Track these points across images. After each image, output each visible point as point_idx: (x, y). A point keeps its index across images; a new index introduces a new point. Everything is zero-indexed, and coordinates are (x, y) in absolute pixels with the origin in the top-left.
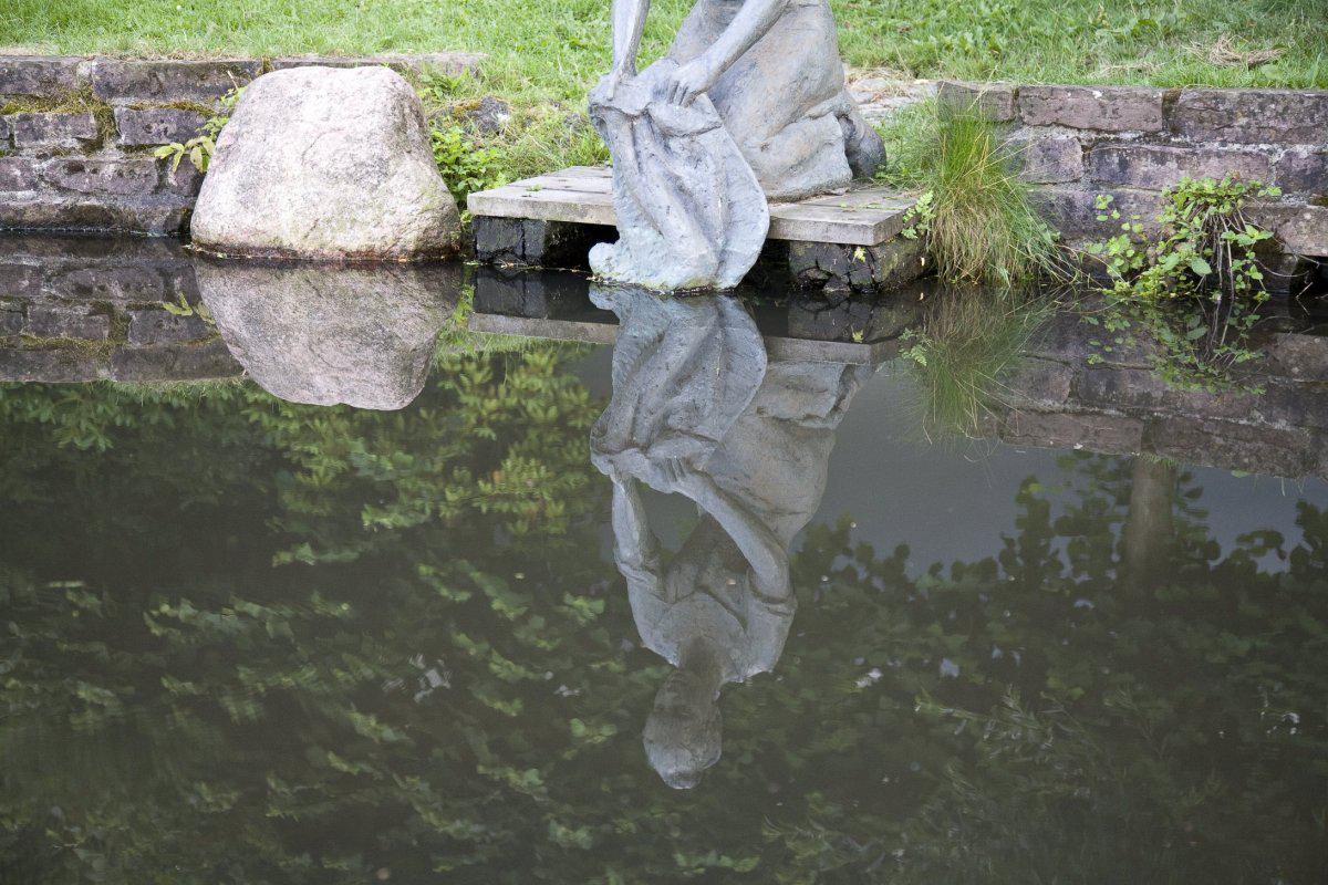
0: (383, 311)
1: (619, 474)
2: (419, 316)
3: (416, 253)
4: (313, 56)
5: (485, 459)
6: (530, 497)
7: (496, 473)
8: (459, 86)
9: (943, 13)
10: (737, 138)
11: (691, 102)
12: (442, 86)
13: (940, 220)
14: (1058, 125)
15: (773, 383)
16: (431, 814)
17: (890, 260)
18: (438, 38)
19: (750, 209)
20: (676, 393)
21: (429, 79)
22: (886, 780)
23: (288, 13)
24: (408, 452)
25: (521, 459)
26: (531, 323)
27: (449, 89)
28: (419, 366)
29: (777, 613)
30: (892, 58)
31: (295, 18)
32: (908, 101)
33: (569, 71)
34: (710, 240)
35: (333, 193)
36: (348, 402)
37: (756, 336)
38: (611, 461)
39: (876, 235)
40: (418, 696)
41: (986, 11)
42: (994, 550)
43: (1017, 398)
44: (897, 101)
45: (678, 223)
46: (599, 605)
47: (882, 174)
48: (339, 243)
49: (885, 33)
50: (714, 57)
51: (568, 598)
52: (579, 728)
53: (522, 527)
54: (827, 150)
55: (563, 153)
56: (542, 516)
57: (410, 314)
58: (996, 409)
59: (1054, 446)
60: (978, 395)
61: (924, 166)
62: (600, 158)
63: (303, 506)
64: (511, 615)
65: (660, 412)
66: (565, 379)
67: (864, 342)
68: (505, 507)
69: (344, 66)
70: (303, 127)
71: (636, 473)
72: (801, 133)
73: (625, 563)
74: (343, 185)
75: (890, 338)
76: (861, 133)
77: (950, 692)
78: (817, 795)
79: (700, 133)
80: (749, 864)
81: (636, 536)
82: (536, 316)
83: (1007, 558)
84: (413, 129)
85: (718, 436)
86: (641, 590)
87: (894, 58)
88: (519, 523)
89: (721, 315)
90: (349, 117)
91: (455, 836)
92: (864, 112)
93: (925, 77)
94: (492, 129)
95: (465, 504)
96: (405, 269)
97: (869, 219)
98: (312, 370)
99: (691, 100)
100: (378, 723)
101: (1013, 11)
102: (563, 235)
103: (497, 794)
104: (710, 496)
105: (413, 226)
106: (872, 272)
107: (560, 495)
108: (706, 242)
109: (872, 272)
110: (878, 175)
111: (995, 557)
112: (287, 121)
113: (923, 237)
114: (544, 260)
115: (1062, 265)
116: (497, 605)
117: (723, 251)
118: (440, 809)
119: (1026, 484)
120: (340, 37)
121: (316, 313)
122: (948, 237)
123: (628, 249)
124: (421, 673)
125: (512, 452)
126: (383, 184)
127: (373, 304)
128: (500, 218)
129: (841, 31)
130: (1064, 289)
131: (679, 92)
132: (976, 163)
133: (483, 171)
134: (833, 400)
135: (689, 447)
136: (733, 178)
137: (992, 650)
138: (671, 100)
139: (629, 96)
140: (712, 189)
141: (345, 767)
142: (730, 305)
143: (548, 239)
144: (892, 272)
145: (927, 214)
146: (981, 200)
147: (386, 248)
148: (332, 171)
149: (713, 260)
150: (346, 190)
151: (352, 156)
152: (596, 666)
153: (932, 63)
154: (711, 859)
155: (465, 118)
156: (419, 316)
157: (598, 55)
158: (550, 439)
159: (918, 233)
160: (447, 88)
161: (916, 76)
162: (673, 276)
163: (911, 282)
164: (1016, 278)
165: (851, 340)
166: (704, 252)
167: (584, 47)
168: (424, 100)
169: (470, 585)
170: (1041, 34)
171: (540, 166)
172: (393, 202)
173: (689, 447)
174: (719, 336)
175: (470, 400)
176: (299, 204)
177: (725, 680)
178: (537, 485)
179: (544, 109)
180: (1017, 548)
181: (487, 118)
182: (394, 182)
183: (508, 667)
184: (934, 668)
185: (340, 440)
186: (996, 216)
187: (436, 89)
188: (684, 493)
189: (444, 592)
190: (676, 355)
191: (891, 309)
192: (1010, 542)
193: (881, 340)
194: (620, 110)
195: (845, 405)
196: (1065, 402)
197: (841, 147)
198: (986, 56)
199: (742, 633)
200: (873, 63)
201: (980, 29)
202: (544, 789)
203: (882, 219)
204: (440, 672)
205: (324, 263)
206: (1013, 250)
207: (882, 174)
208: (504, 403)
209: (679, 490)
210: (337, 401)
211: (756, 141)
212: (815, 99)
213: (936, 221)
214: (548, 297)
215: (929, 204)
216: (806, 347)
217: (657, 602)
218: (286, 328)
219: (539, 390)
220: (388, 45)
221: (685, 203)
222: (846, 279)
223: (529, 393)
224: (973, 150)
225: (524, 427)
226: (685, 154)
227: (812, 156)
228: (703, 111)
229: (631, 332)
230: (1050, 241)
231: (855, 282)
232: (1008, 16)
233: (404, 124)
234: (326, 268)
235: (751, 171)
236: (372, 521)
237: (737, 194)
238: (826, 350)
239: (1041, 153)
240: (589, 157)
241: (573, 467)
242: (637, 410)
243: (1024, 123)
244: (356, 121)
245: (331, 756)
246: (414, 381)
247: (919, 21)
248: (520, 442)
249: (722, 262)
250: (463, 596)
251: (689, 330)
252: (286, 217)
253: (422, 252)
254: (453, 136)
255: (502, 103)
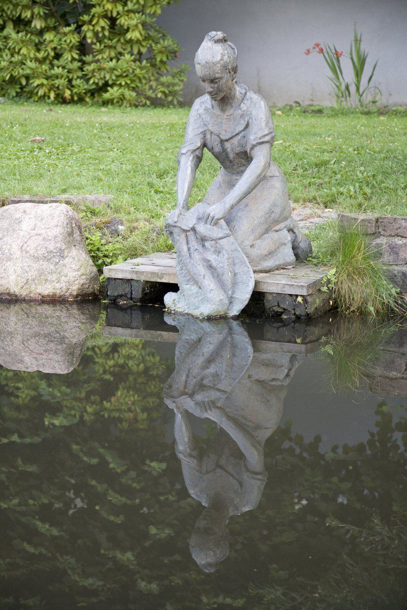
0: (60, 324)
1: (178, 408)
2: (79, 327)
3: (77, 296)
4: (27, 197)
5: (107, 391)
6: (130, 410)
7: (113, 397)
8: (99, 212)
9: (339, 176)
10: (239, 241)
11: (216, 224)
12: (91, 212)
13: (339, 282)
14: (398, 236)
15: (256, 362)
16: (76, 576)
17: (315, 302)
18: (89, 188)
19: (245, 276)
20: (208, 368)
21: (85, 208)
22: (310, 557)
23: (15, 175)
24: (68, 387)
25: (125, 391)
26: (134, 331)
27: (94, 213)
28: (78, 352)
29: (257, 479)
30: (314, 199)
31: (18, 177)
32: (322, 220)
33: (154, 204)
34: (225, 292)
35: (35, 266)
36: (41, 370)
37: (247, 340)
38: (174, 402)
39: (308, 290)
40: (71, 512)
41: (360, 175)
42: (365, 439)
43: (378, 371)
44: (317, 220)
45: (209, 283)
46: (164, 466)
47: (310, 259)
48: (38, 291)
49: (310, 186)
50: (227, 202)
51: (148, 462)
52: (153, 530)
53: (125, 425)
54: (283, 247)
55: (151, 245)
56: (136, 420)
57: (74, 327)
58: (368, 376)
59: (397, 395)
60: (359, 369)
61: (331, 255)
62: (170, 248)
63: (14, 414)
64: (119, 471)
65: (199, 378)
66: (148, 350)
67: (302, 343)
68: (117, 415)
69: (42, 202)
70: (22, 233)
71: (187, 407)
72: (270, 239)
73: (180, 453)
74: (41, 262)
75: (315, 341)
76: (300, 238)
77: (342, 513)
78: (274, 565)
79: (220, 239)
80: (240, 603)
81: (186, 440)
82: (137, 328)
83: (371, 443)
84: (77, 235)
85: (229, 389)
86: (188, 465)
87: (315, 198)
88: (124, 423)
89: (230, 329)
90: (45, 228)
91: (88, 587)
92: (300, 226)
93: (330, 208)
94: (116, 233)
95: (96, 414)
96: (71, 304)
97: (304, 282)
98: (23, 354)
99: (216, 223)
100: (50, 527)
101: (374, 176)
102: (151, 287)
103: (110, 565)
104: (224, 419)
105: (76, 282)
106: (306, 308)
107: (144, 409)
108: (223, 292)
109: (306, 308)
110: (308, 259)
111: (365, 442)
112: (14, 230)
113: (331, 291)
114: (141, 300)
115: (401, 305)
116: (111, 466)
117: (232, 297)
118: (81, 573)
119: (381, 405)
120: (40, 187)
121: (26, 326)
122: (344, 290)
123: (184, 295)
124: (72, 500)
125: (121, 387)
126: (61, 262)
127: (55, 321)
128: (120, 279)
129: (289, 184)
130: (402, 317)
131: (210, 219)
132: (358, 254)
133: (111, 254)
134: (286, 371)
135: (213, 395)
136: (237, 261)
137: (363, 491)
138: (206, 223)
139: (184, 221)
140: (226, 267)
141: (32, 550)
142: (235, 324)
143: (144, 290)
144: (316, 308)
145: (333, 279)
146: (360, 273)
147: (62, 294)
148: (36, 255)
149: (227, 301)
150: (43, 265)
151: (46, 248)
152: (162, 498)
153: (334, 201)
154: (220, 599)
155: (103, 228)
156: (79, 327)
157: (168, 196)
158: (140, 380)
159: (328, 289)
160: (93, 213)
161: (326, 207)
162: (206, 309)
163: (325, 313)
164: (377, 311)
165: (295, 342)
166: (222, 298)
167: (161, 192)
168: (82, 218)
169: (99, 455)
170: (388, 188)
171: (139, 252)
172: (66, 271)
173: (213, 395)
174: (229, 339)
175: (100, 360)
176: (19, 271)
177: (231, 514)
178: (133, 403)
179: (142, 224)
180: (376, 438)
181: (113, 228)
182: (67, 260)
183: (117, 498)
184: (335, 500)
185: (34, 381)
186: (367, 280)
187: (88, 213)
188: (211, 418)
189: (85, 459)
190: (207, 349)
191: (315, 326)
192: (372, 434)
193: (310, 342)
194: (180, 227)
195: (292, 373)
196: (403, 374)
197: (290, 245)
198: (360, 199)
199: (239, 490)
200: (305, 201)
201: (357, 184)
202: (135, 562)
203: (311, 282)
204: (82, 500)
205: (31, 301)
206: (376, 298)
207: (310, 259)
208: (117, 362)
209: (208, 417)
210: (36, 369)
211: (247, 243)
212: (277, 222)
213: (337, 283)
214: (143, 319)
215: (334, 275)
216: (272, 345)
217: (197, 473)
218: (10, 333)
219: (135, 356)
220: (64, 191)
221: (213, 274)
222: (293, 312)
223: (129, 357)
224: (356, 248)
225: (127, 375)
226: (213, 249)
227: (276, 250)
228: (222, 228)
229: (184, 337)
230: (395, 294)
231: (297, 313)
232: (371, 178)
233: (72, 232)
234: (32, 303)
235: (245, 258)
236: (49, 422)
237: (238, 269)
238: (283, 347)
239: (390, 250)
240: (164, 248)
241: (151, 395)
242: (188, 376)
243: (381, 235)
244: (48, 230)
245: (25, 544)
246: (75, 359)
247: (327, 180)
248: (125, 382)
249: (231, 303)
250: (95, 461)
251: (214, 337)
252: (13, 277)
253: (80, 295)
254: (96, 237)
255: (121, 220)
